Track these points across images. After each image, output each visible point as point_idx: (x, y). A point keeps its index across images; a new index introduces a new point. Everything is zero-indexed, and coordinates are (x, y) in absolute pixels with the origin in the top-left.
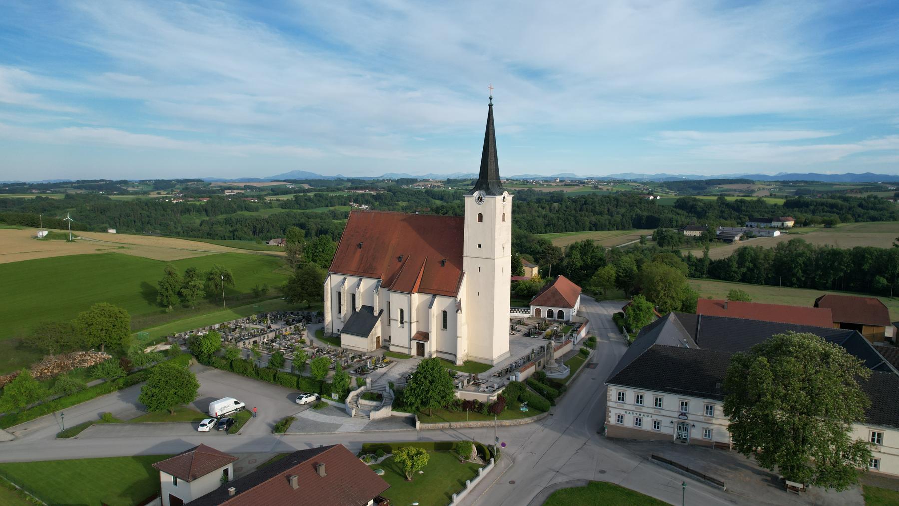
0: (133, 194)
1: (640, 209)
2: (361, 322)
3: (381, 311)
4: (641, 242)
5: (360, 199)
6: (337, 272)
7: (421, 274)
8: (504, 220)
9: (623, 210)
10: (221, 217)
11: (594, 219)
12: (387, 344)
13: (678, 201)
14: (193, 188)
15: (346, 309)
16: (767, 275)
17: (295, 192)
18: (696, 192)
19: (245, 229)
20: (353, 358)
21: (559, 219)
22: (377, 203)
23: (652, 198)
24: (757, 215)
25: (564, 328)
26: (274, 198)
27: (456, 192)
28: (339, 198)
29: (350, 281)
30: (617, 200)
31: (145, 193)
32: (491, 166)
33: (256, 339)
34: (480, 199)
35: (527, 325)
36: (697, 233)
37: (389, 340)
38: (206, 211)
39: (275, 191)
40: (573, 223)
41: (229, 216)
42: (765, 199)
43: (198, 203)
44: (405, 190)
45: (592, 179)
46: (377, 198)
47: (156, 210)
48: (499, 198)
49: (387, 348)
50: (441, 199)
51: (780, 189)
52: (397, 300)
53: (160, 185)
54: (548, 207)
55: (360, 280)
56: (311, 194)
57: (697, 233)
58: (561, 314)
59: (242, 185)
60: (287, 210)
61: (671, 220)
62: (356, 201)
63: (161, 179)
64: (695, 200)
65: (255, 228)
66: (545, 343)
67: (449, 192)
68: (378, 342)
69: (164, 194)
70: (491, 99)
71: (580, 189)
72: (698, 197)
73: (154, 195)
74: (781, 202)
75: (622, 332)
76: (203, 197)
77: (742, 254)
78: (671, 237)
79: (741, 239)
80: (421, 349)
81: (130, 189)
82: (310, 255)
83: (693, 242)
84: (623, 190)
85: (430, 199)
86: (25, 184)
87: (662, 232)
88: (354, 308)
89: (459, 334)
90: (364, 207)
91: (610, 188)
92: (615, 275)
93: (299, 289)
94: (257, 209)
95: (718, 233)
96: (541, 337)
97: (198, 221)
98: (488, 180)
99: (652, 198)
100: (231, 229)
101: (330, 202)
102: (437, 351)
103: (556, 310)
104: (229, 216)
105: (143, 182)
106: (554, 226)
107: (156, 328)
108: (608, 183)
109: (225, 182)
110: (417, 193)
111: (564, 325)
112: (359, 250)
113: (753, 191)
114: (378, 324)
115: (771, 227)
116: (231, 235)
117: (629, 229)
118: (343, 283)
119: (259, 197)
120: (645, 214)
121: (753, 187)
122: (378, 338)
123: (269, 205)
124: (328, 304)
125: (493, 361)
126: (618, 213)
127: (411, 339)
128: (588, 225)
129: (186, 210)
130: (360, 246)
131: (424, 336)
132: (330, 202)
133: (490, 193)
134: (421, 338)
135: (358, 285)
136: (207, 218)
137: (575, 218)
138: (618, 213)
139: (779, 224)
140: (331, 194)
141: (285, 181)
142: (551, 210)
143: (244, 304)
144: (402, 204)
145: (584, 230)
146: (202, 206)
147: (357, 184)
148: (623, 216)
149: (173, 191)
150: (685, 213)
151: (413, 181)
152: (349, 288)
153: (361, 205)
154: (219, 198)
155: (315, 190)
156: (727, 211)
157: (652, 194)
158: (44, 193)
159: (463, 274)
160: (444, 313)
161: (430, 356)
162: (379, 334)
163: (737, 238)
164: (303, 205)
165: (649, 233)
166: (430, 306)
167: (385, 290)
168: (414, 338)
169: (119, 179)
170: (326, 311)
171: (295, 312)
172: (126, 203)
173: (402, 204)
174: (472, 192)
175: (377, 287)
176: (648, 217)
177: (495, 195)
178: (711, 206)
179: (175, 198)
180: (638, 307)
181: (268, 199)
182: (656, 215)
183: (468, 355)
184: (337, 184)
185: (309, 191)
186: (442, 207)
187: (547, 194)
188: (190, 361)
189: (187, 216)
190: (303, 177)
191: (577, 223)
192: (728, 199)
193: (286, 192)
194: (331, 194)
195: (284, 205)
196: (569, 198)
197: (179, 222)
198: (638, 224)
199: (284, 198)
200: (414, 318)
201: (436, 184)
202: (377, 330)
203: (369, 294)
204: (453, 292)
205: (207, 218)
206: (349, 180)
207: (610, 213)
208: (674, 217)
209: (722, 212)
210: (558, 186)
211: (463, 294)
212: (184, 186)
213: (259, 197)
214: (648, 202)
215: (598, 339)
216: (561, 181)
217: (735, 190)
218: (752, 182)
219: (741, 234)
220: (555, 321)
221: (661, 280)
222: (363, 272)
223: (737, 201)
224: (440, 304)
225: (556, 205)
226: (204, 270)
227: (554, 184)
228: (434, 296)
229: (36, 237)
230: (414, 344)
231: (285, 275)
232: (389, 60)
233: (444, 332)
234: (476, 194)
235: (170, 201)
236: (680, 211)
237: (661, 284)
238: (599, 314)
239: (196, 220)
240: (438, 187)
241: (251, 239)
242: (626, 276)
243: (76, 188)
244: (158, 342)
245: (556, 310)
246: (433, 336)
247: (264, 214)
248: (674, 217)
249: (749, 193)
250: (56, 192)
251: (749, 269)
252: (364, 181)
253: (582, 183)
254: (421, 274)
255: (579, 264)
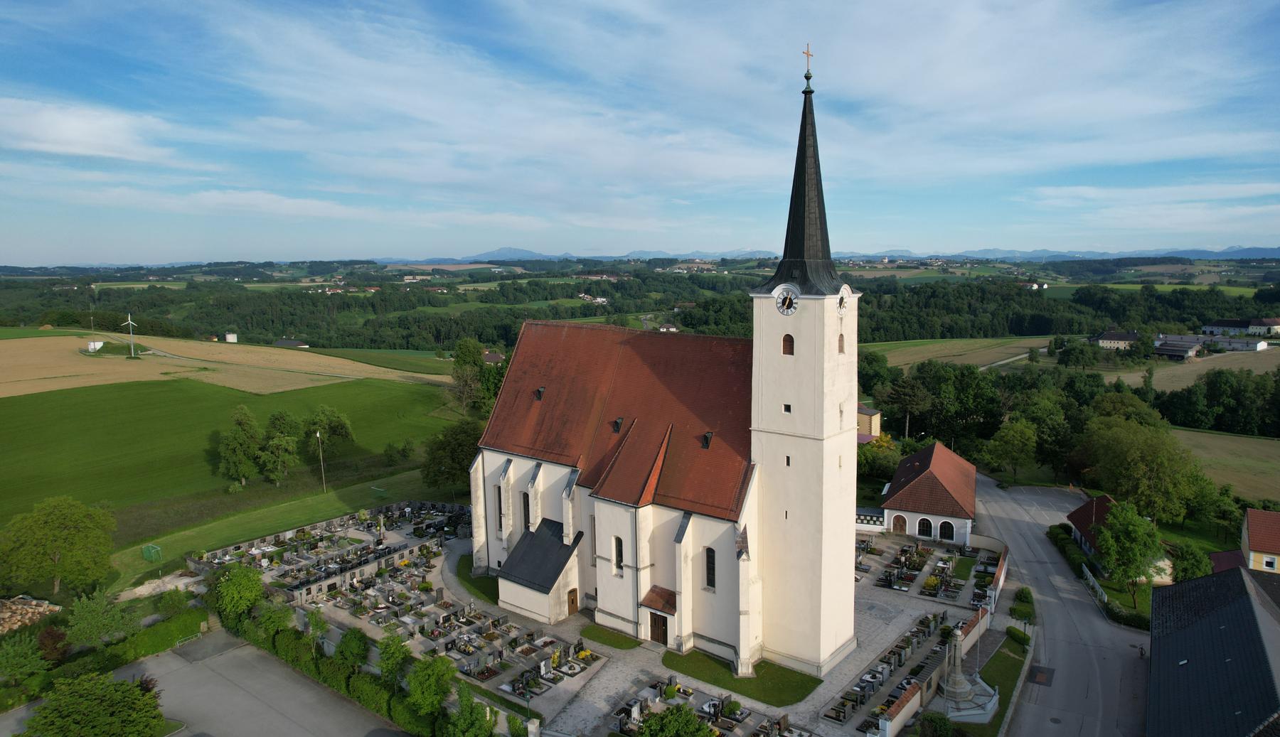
0: (276, 281)
1: (1020, 304)
2: (540, 555)
3: (579, 536)
4: (1031, 359)
5: (594, 288)
6: (497, 447)
7: (659, 462)
8: (841, 350)
9: (992, 307)
10: (393, 316)
11: (947, 320)
12: (591, 604)
13: (1078, 291)
14: (359, 272)
15: (511, 523)
16: (1262, 419)
17: (503, 278)
18: (1099, 277)
19: (424, 334)
20: (514, 643)
21: (893, 319)
22: (618, 295)
23: (1035, 287)
24: (1211, 314)
25: (959, 563)
26: (471, 287)
27: (734, 278)
28: (563, 287)
29: (519, 467)
30: (982, 290)
31: (295, 280)
32: (811, 229)
33: (336, 580)
34: (787, 303)
35: (880, 553)
36: (1122, 345)
37: (595, 598)
38: (373, 306)
39: (474, 277)
40: (916, 326)
41: (405, 313)
42: (1221, 288)
43: (362, 295)
44: (659, 274)
45: (937, 258)
46: (618, 287)
47: (302, 304)
48: (831, 301)
49: (589, 612)
50: (713, 288)
51: (1237, 272)
52: (610, 519)
53: (317, 268)
54: (875, 302)
55: (538, 466)
56: (524, 282)
57: (1122, 345)
58: (947, 530)
59: (429, 268)
60: (488, 305)
61: (1070, 323)
62: (587, 292)
63: (318, 259)
64: (1106, 290)
65: (438, 332)
66: (929, 608)
67: (724, 278)
68: (572, 601)
69: (319, 280)
70: (808, 78)
71: (920, 273)
72: (1110, 286)
73: (305, 283)
74: (1250, 292)
75: (1080, 575)
76: (370, 286)
77: (1214, 382)
78: (1082, 352)
79: (1199, 354)
80: (659, 628)
81: (277, 275)
82: (492, 387)
83: (1118, 359)
84: (987, 275)
85: (696, 288)
86: (141, 268)
87: (1063, 341)
88: (527, 527)
89: (742, 607)
90: (600, 300)
91: (966, 272)
92: (1035, 438)
93: (448, 461)
94: (445, 304)
95: (1157, 344)
96: (914, 590)
97: (361, 321)
98: (804, 260)
99: (1035, 287)
100: (405, 333)
101: (551, 293)
102: (696, 635)
103: (936, 522)
104: (405, 313)
105: (294, 265)
106: (886, 330)
107: (188, 532)
108: (963, 264)
109: (406, 264)
110: (677, 279)
111: (957, 556)
112: (537, 404)
113: (1192, 276)
114: (573, 563)
115: (1248, 335)
116: (404, 342)
117: (1003, 336)
118: (506, 470)
119: (450, 286)
120: (1028, 312)
121: (1191, 269)
122: (573, 592)
123: (463, 298)
124: (479, 510)
125: (819, 667)
126: (985, 311)
127: (639, 605)
128: (939, 329)
129: (345, 304)
130: (538, 394)
131: (665, 600)
132: (551, 293)
133: (809, 288)
134: (661, 603)
135: (534, 478)
136: (372, 317)
137: (919, 318)
138: (985, 311)
139: (1263, 330)
140: (552, 281)
141: (490, 262)
142: (880, 306)
143: (362, 480)
144: (654, 295)
145: (933, 337)
146: (368, 299)
147: (591, 266)
148: (993, 314)
149: (332, 277)
150: (1091, 310)
151: (671, 262)
152: (518, 481)
153: (595, 298)
154: (393, 286)
155: (530, 276)
156: (1160, 309)
157: (1035, 282)
158: (164, 280)
159: (748, 470)
160: (710, 553)
161: (680, 645)
162: (575, 584)
163: (1191, 353)
164: (511, 297)
165: (1041, 343)
166: (679, 538)
167: (586, 492)
168: (647, 603)
169: (262, 261)
170: (475, 523)
171: (439, 505)
172: (262, 295)
173: (654, 295)
174: (767, 286)
175: (569, 485)
176: (1033, 317)
177: (823, 294)
178: (1133, 300)
179: (331, 287)
180: (1128, 534)
181: (461, 289)
182: (1046, 314)
183: (762, 648)
184: (563, 266)
185: (521, 277)
186: (714, 301)
187: (871, 281)
188: (203, 626)
189: (346, 313)
190: (515, 257)
191: (922, 326)
192: (1159, 288)
193: (490, 278)
194: (552, 281)
195: (485, 297)
196: (905, 287)
197: (334, 322)
198: (1019, 327)
199: (483, 287)
200: (645, 557)
201: (706, 267)
202: (571, 576)
203: (553, 496)
204: (728, 510)
205: (372, 317)
206: (580, 261)
207: (972, 311)
208: (1075, 316)
209: (1151, 309)
210: (886, 268)
211: (751, 515)
212: (349, 270)
213: (450, 286)
214: (1031, 293)
215: (1035, 595)
216: (890, 262)
217: (1162, 275)
218: (1190, 262)
219: (1198, 347)
220: (935, 544)
221: (1143, 459)
222: (544, 451)
223: (1174, 291)
224: (700, 533)
225: (887, 297)
226: (299, 417)
227: (880, 266)
228: (688, 514)
229: (85, 352)
230: (645, 614)
231: (424, 429)
232: (638, 92)
233: (709, 595)
234: (779, 292)
235: (324, 292)
236: (1083, 308)
237: (1142, 466)
238: (1014, 522)
239: (358, 319)
240: (708, 270)
241: (432, 349)
242: (1057, 442)
243: (205, 273)
244: (167, 570)
245: (936, 522)
246: (686, 601)
247: (455, 311)
248: (1075, 316)
249: (1188, 278)
250: (178, 280)
251: (1228, 409)
252: (601, 262)
253: (922, 263)
254: (659, 462)
255: (953, 409)
